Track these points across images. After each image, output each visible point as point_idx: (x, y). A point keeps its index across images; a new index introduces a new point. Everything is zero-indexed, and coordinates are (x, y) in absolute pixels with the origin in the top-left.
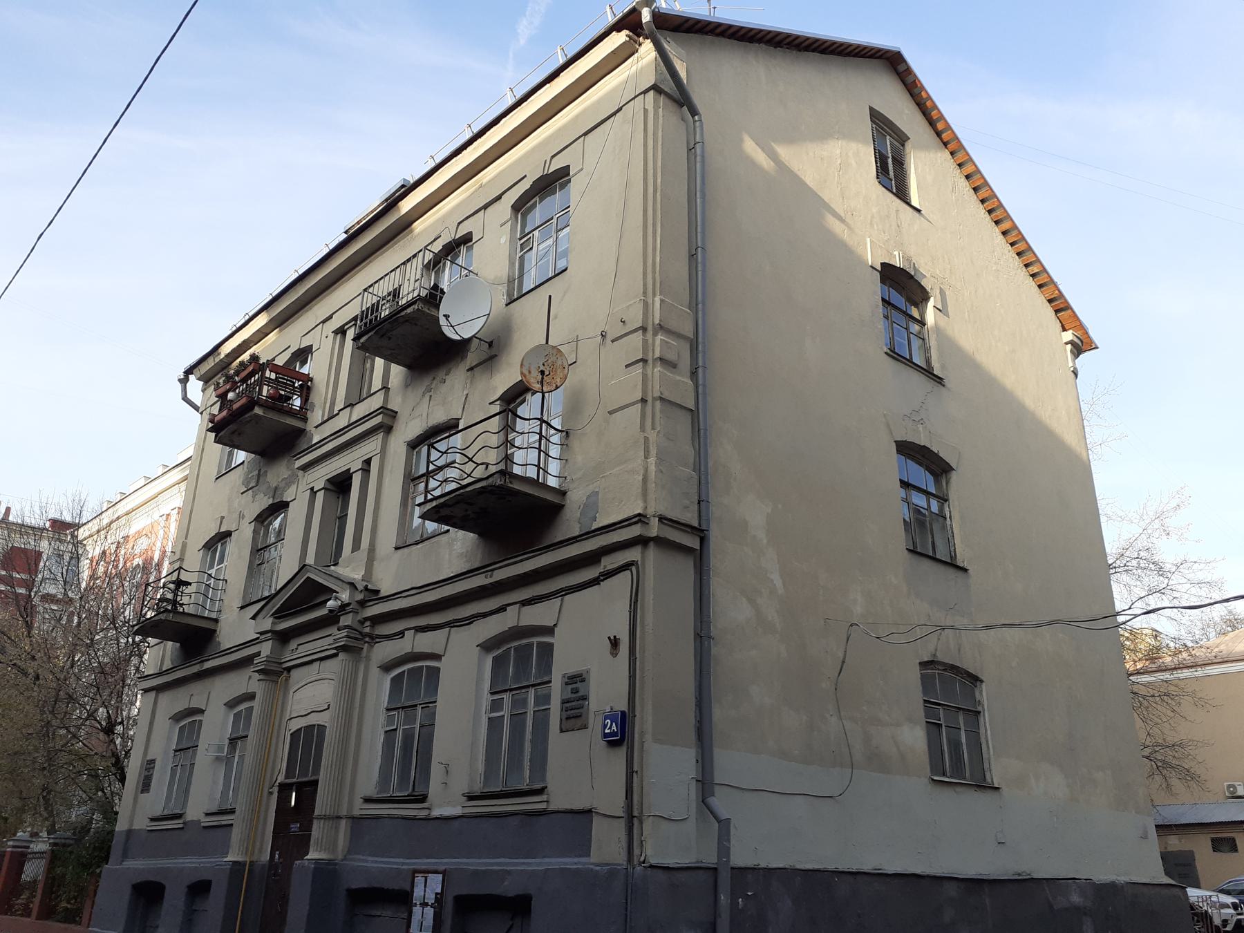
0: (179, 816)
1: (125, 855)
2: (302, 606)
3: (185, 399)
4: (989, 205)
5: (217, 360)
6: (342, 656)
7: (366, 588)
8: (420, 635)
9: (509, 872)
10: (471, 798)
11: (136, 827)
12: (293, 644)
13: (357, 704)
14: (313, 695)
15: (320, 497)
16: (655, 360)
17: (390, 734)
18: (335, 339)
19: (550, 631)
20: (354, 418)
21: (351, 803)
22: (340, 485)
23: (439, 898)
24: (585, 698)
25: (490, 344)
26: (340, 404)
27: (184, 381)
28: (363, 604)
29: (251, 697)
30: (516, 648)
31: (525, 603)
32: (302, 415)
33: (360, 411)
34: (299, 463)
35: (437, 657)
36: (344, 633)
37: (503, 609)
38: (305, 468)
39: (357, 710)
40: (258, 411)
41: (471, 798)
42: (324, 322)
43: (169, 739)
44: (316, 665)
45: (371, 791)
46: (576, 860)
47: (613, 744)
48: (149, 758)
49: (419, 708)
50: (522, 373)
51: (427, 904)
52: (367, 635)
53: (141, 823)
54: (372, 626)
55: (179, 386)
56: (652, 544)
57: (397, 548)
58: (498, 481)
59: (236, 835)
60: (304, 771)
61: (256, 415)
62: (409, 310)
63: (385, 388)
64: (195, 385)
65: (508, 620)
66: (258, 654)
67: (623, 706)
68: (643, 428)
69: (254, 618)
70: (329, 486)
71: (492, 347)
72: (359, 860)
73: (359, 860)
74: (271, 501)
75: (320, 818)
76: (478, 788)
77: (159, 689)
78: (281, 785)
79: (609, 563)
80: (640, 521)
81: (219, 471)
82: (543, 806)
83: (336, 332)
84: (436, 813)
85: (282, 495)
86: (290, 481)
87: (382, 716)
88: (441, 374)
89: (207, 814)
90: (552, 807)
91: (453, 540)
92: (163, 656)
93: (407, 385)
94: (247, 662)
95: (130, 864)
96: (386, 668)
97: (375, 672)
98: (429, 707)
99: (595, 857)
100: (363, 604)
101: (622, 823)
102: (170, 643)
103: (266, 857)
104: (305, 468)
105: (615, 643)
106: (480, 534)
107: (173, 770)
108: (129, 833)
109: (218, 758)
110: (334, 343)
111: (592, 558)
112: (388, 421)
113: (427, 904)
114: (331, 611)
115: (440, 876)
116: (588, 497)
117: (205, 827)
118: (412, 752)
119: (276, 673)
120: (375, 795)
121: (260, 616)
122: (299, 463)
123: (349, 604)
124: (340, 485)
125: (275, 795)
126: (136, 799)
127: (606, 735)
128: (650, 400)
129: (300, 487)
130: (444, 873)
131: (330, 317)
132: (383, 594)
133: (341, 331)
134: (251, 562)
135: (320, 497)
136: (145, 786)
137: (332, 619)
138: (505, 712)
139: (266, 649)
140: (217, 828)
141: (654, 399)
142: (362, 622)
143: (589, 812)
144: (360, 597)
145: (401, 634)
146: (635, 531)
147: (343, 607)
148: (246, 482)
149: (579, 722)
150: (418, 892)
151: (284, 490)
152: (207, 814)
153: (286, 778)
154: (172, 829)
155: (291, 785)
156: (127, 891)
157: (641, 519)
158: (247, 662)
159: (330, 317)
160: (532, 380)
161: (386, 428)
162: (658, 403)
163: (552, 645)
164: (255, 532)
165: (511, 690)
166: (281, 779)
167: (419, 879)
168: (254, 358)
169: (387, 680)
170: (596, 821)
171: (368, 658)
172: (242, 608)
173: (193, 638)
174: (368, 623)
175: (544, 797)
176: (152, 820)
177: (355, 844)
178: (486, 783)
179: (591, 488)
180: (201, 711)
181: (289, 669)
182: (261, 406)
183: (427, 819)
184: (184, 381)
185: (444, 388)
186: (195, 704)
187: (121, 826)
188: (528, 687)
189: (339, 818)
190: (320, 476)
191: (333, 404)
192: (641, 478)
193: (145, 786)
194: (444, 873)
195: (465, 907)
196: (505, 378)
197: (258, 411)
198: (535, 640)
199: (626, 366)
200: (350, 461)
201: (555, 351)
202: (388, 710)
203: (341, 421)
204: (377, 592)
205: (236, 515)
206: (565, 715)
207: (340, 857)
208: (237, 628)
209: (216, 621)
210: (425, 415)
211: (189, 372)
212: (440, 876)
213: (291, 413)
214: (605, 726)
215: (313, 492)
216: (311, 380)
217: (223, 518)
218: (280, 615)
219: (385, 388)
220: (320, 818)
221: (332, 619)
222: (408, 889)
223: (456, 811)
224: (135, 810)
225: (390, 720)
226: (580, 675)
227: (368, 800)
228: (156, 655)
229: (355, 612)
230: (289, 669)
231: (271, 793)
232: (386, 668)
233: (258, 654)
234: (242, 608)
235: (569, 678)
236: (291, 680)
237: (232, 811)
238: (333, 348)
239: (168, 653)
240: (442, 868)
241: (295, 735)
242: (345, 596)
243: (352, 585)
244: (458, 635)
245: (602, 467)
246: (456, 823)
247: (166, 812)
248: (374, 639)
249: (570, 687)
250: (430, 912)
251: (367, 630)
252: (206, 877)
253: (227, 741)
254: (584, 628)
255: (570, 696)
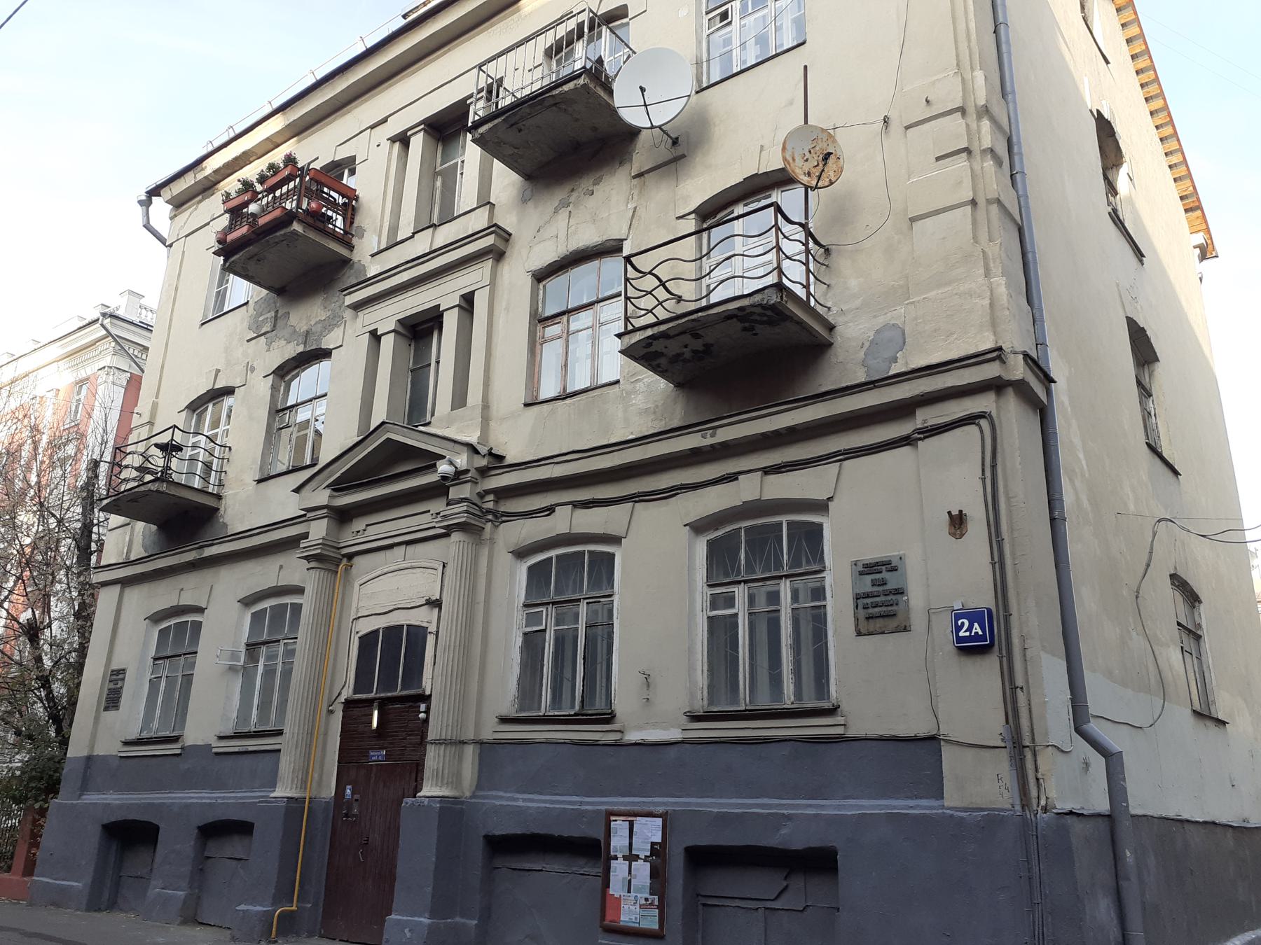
0: (175, 739)
1: (84, 787)
2: (385, 473)
3: (148, 227)
4: (1145, 77)
5: (200, 176)
6: (456, 537)
7: (490, 454)
8: (581, 513)
9: (789, 817)
10: (695, 718)
11: (100, 751)
12: (359, 524)
13: (481, 597)
14: (395, 586)
15: (388, 343)
16: (984, 151)
17: (532, 642)
18: (391, 148)
19: (821, 507)
20: (439, 242)
21: (478, 725)
22: (420, 329)
23: (657, 851)
24: (900, 592)
25: (675, 142)
26: (404, 231)
27: (146, 203)
28: (484, 472)
29: (300, 591)
30: (747, 529)
31: (767, 471)
32: (346, 240)
33: (445, 234)
34: (350, 300)
35: (200, 610)
36: (463, 507)
37: (732, 478)
38: (358, 307)
39: (481, 606)
40: (296, 226)
41: (695, 718)
42: (373, 127)
43: (146, 644)
44: (399, 551)
45: (508, 709)
46: (911, 803)
47: (971, 649)
48: (114, 666)
49: (282, 643)
50: (785, 159)
51: (637, 857)
52: (489, 511)
53: (108, 746)
54: (496, 502)
55: (139, 210)
56: (1010, 391)
57: (526, 405)
58: (774, 298)
59: (286, 764)
60: (388, 680)
61: (295, 233)
62: (566, 88)
63: (485, 202)
64: (160, 207)
65: (748, 489)
66: (305, 536)
67: (984, 599)
68: (975, 239)
69: (297, 490)
70: (400, 329)
71: (679, 148)
72: (501, 798)
73: (501, 798)
74: (301, 349)
75: (438, 742)
76: (700, 705)
77: (125, 582)
78: (348, 704)
79: (927, 416)
80: (999, 357)
81: (205, 316)
82: (840, 730)
83: (393, 140)
84: (633, 736)
85: (319, 341)
86: (329, 325)
87: (519, 616)
88: (586, 183)
89: (221, 738)
90: (851, 733)
91: (629, 393)
92: (131, 541)
93: (524, 200)
94: (291, 544)
95: (92, 798)
96: (521, 554)
97: (504, 558)
98: (602, 601)
99: (953, 798)
100: (484, 472)
101: (1004, 755)
102: (140, 525)
103: (330, 791)
104: (358, 307)
105: (958, 522)
106: (679, 385)
107: (154, 685)
108: (89, 759)
109: (232, 669)
110: (390, 153)
111: (904, 409)
112: (500, 245)
113: (637, 857)
114: (444, 478)
115: (659, 821)
116: (877, 332)
117: (217, 754)
118: (572, 662)
119: (332, 561)
120: (514, 715)
121: (308, 487)
122: (350, 300)
123: (467, 471)
124: (420, 329)
125: (339, 715)
126: (97, 718)
127: (960, 639)
128: (981, 202)
129: (349, 331)
130: (663, 816)
131: (385, 120)
132: (509, 460)
133: (403, 140)
134: (269, 426)
135: (388, 343)
136: (112, 700)
137: (439, 490)
138: (741, 608)
139: (318, 530)
140: (251, 749)
141: (989, 202)
142: (481, 496)
143: (933, 738)
144: (483, 462)
145: (550, 510)
146: (990, 371)
147: (459, 474)
148: (255, 325)
149: (892, 623)
150: (618, 842)
151: (321, 335)
152: (221, 738)
153: (356, 691)
154: (159, 755)
155: (370, 702)
156: (100, 828)
157: (997, 354)
158: (291, 544)
159: (385, 120)
160: (798, 171)
161: (498, 254)
162: (994, 209)
163: (820, 526)
164: (274, 388)
165: (745, 582)
166: (348, 693)
167: (619, 827)
168: (290, 160)
169: (522, 571)
170: (947, 752)
171: (492, 541)
172: (259, 481)
173: (182, 520)
174: (491, 497)
175: (840, 720)
176: (126, 743)
177: (486, 776)
178: (711, 703)
179: (881, 321)
180: (616, 540)
181: (350, 557)
182: (300, 221)
183: (617, 745)
184: (146, 203)
185: (591, 202)
186: (186, 600)
187: (76, 749)
188: (780, 577)
189: (463, 743)
190: (387, 316)
191: (394, 229)
192: (987, 302)
193: (112, 700)
194: (663, 816)
195: (702, 864)
196: (702, 184)
197: (296, 226)
198: (784, 519)
199: (938, 159)
200: (444, 294)
201: (825, 136)
202: (526, 606)
203: (421, 245)
204: (501, 458)
205: (240, 368)
206: (862, 613)
207: (468, 794)
208: (249, 505)
209: (219, 497)
210: (562, 235)
211: (155, 192)
212: (659, 821)
213: (333, 236)
214: (959, 628)
215: (375, 337)
216: (357, 199)
217: (218, 371)
218: (339, 486)
219: (485, 202)
220: (438, 742)
221: (439, 490)
222: (602, 838)
223: (674, 734)
224: (97, 733)
225: (532, 619)
226: (889, 563)
227: (504, 720)
228: (122, 539)
229: (474, 482)
230: (350, 557)
231: (331, 712)
232: (521, 554)
233: (305, 536)
234: (259, 481)
235: (866, 566)
236: (354, 571)
237: (279, 733)
238: (389, 160)
239: (138, 539)
240: (660, 810)
241: (368, 641)
242: (462, 461)
243: (473, 449)
244: (647, 513)
245: (900, 296)
246: (672, 752)
247: (145, 735)
248: (500, 517)
249: (868, 578)
250: (643, 870)
251: (490, 505)
252: (248, 818)
253: (243, 648)
254: (876, 507)
255: (868, 588)
